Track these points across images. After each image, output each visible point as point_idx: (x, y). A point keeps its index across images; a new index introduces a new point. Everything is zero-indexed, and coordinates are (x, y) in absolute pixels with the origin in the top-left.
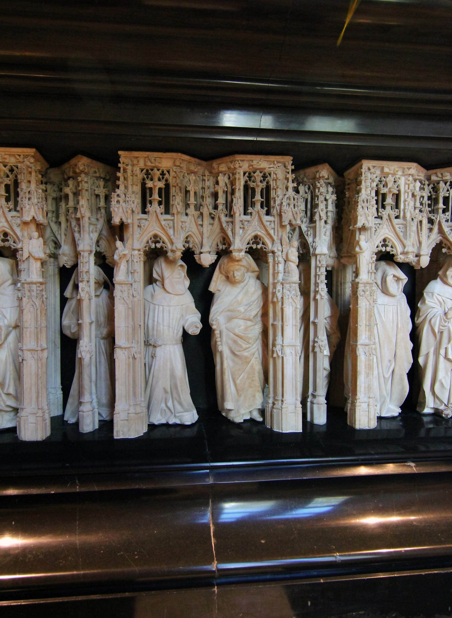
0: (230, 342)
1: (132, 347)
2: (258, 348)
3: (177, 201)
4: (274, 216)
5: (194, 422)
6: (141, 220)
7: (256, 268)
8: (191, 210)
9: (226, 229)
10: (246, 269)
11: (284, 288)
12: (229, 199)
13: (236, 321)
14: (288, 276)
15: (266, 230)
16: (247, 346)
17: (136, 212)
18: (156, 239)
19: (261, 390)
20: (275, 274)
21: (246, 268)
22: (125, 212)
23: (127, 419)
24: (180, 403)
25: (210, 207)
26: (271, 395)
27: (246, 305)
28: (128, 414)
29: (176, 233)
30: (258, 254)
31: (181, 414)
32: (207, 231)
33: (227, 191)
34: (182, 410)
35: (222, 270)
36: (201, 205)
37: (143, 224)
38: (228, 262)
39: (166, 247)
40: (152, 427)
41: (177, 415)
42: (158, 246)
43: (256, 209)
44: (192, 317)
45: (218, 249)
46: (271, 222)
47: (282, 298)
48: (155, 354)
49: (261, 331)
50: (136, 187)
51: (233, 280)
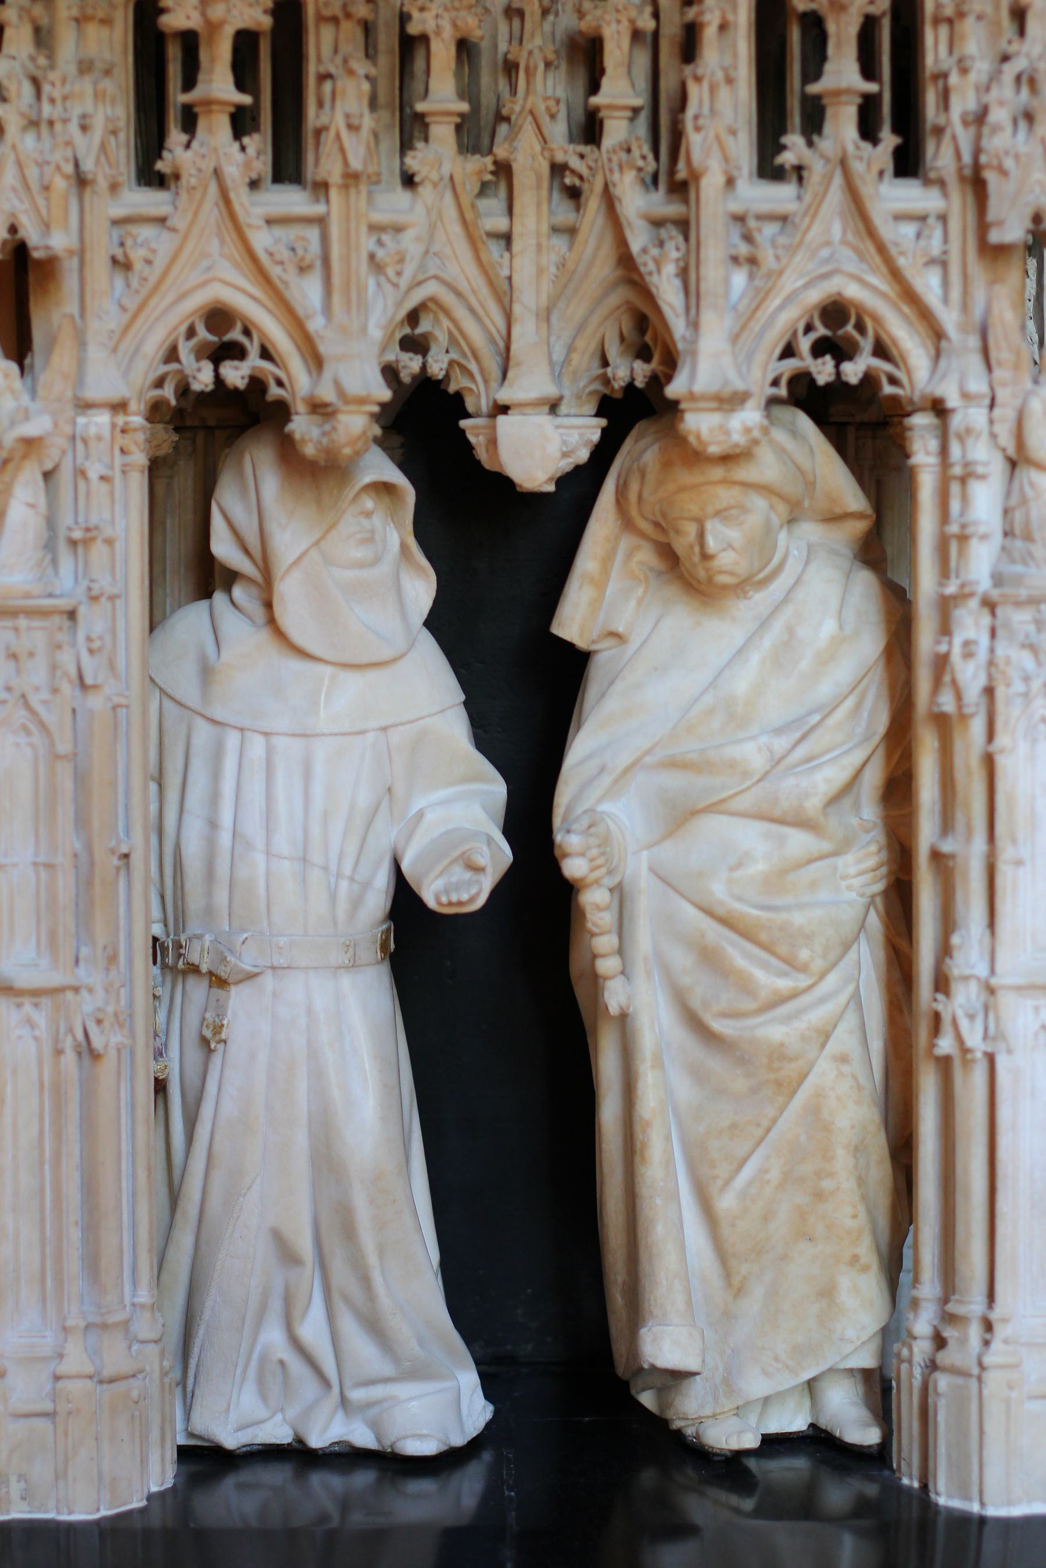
0: (681, 959)
1: (76, 990)
2: (856, 996)
3: (344, 110)
4: (942, 183)
5: (459, 1440)
6: (134, 229)
7: (852, 497)
8: (439, 154)
9: (646, 264)
10: (782, 508)
11: (1000, 632)
12: (668, 83)
13: (714, 827)
14: (1027, 558)
15: (895, 274)
16: (784, 984)
17: (102, 184)
18: (222, 334)
19: (867, 1251)
20: (951, 545)
21: (782, 497)
22: (35, 186)
23: (49, 1406)
24: (375, 1328)
25: (558, 131)
26: (929, 1288)
27: (779, 731)
28: (57, 1378)
29: (336, 298)
30: (857, 416)
31: (378, 1392)
32: (540, 271)
33: (656, 34)
34: (387, 1369)
35: (634, 512)
36: (501, 118)
37: (142, 252)
38: (667, 465)
39: (280, 383)
40: (204, 1461)
41: (357, 1395)
42: (235, 374)
43: (826, 144)
44: (445, 802)
45: (606, 381)
46: (923, 218)
47: (989, 691)
48: (218, 1029)
49: (880, 887)
50: (105, 32)
51: (701, 574)
